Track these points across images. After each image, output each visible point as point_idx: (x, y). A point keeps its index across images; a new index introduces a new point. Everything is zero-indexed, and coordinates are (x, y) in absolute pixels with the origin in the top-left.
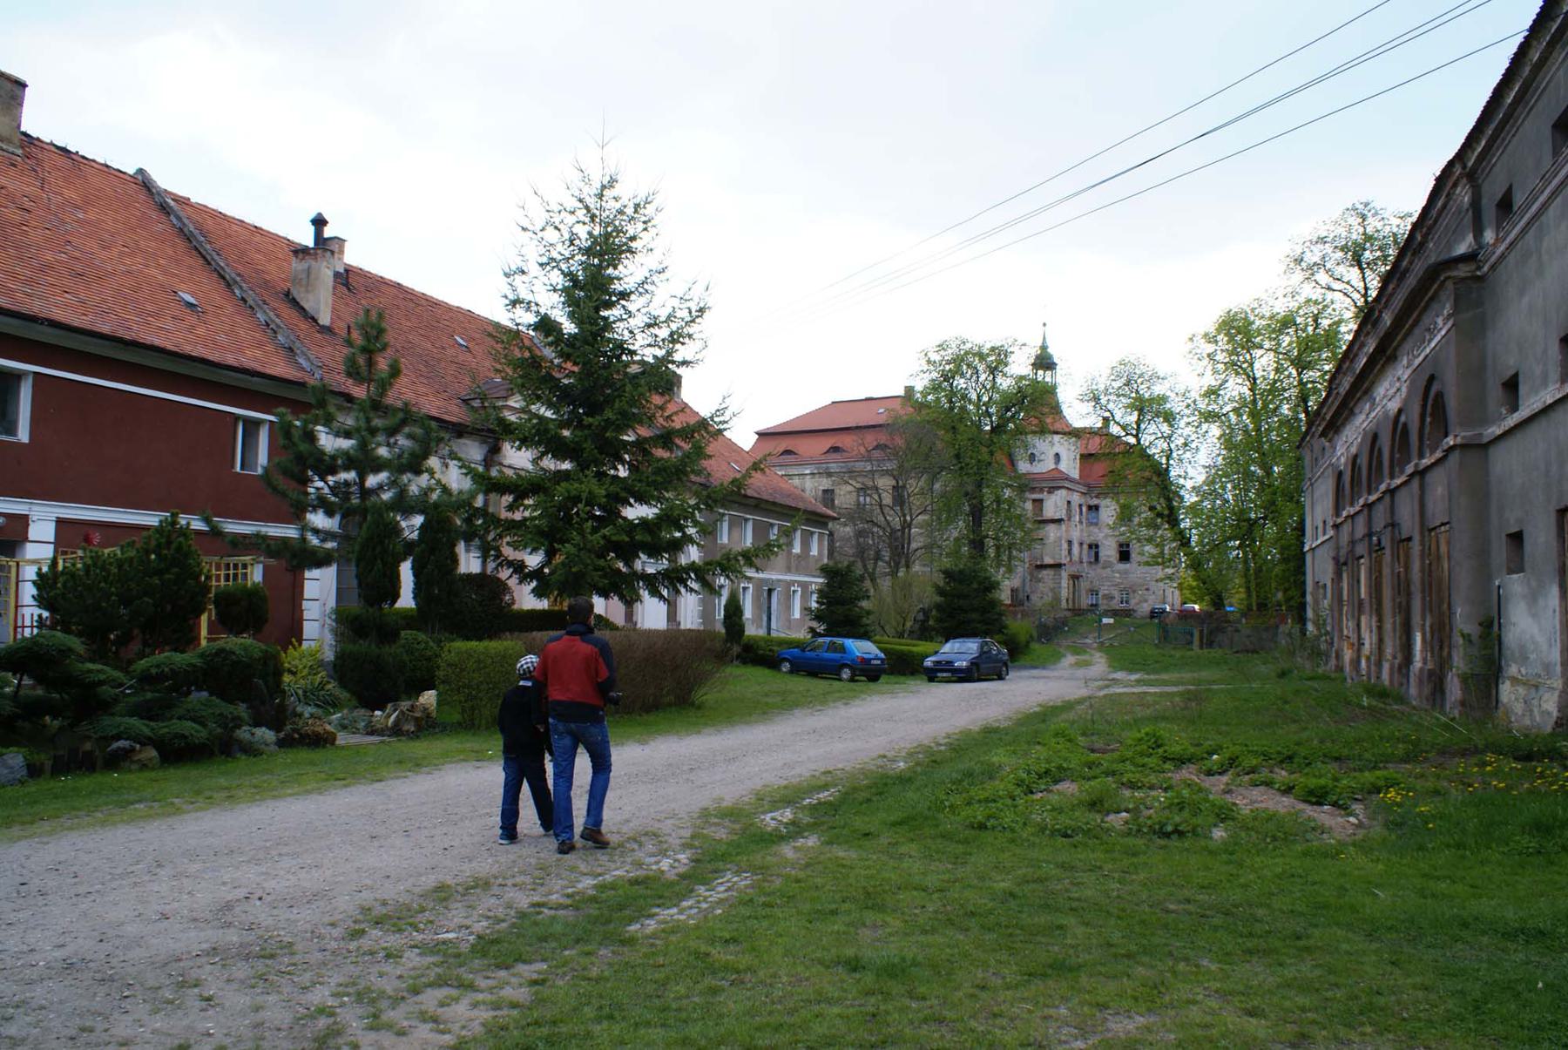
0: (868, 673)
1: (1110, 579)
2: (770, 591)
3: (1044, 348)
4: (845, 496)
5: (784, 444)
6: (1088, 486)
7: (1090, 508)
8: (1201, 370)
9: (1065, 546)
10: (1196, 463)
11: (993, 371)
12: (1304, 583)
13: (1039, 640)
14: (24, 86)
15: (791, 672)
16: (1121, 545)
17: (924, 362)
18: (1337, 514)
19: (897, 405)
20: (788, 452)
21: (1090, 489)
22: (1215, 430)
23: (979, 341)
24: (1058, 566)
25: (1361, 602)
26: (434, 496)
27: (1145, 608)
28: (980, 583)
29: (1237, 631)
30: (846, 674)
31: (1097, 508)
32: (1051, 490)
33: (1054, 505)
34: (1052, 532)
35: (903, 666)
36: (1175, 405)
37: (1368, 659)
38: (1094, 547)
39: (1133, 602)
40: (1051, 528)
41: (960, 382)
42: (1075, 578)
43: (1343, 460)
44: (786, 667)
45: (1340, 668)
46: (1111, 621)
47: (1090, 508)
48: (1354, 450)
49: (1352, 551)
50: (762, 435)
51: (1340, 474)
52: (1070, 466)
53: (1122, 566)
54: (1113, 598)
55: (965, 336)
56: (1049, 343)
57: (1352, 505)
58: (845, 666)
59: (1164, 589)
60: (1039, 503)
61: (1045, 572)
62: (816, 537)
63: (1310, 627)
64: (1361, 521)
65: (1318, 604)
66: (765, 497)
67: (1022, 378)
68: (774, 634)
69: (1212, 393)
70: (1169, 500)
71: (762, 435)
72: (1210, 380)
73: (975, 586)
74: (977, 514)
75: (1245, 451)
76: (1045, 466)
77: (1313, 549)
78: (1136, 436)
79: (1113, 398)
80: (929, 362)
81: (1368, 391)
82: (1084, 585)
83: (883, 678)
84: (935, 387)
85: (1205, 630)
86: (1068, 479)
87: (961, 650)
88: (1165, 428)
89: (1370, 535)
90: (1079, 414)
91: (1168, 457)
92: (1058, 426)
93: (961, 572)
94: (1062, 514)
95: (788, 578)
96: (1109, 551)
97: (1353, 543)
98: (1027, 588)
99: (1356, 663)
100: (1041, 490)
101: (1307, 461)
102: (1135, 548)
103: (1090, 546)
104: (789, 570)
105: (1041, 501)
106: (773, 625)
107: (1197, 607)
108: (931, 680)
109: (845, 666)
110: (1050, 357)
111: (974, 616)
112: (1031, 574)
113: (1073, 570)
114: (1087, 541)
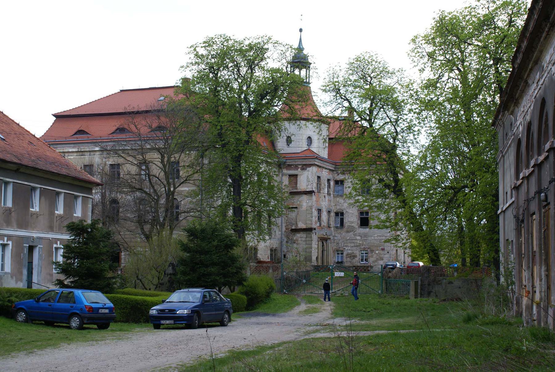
0: (97, 321)
1: (353, 242)
2: (31, 249)
3: (300, 49)
4: (129, 168)
5: (76, 125)
6: (335, 164)
7: (337, 182)
8: (421, 66)
9: (315, 213)
10: (417, 140)
11: (251, 66)
12: (498, 240)
13: (281, 291)
15: (26, 321)
16: (362, 213)
17: (192, 56)
18: (517, 178)
19: (171, 92)
20: (80, 132)
21: (336, 167)
22: (431, 117)
23: (239, 38)
24: (309, 230)
25: (534, 252)
27: (378, 267)
28: (220, 241)
29: (451, 283)
30: (75, 322)
32: (305, 167)
33: (307, 179)
34: (304, 202)
35: (136, 315)
36: (400, 96)
37: (538, 305)
38: (340, 214)
39: (371, 260)
40: (304, 197)
41: (224, 74)
42: (324, 240)
43: (521, 128)
44: (22, 316)
45: (519, 314)
46: (342, 274)
47: (337, 182)
48: (528, 118)
49: (527, 209)
50: (59, 117)
51: (519, 141)
52: (320, 148)
54: (355, 256)
55: (229, 34)
56: (304, 45)
57: (527, 167)
58: (74, 314)
59: (397, 252)
60: (294, 177)
61: (298, 235)
62: (80, 201)
63: (502, 279)
64: (533, 180)
65: (508, 257)
66: (25, 162)
67: (277, 71)
68: (35, 287)
69: (431, 85)
70: (395, 174)
71: (59, 117)
72: (429, 74)
73: (215, 243)
74: (238, 184)
75: (451, 134)
76: (299, 146)
77: (504, 212)
78: (369, 121)
79: (351, 89)
80: (197, 55)
81: (538, 61)
82: (331, 247)
83: (112, 326)
84: (202, 78)
85: (426, 282)
86: (318, 158)
87: (184, 299)
88: (391, 113)
89: (539, 192)
90: (325, 103)
91: (395, 139)
92: (307, 112)
93: (203, 231)
94: (313, 187)
95: (50, 236)
96: (352, 217)
97: (528, 201)
98: (284, 249)
99: (529, 308)
100: (296, 167)
101: (500, 135)
102: (373, 214)
103: (337, 214)
104: (51, 229)
105: (296, 176)
106: (35, 279)
107: (421, 264)
108: (157, 327)
109: (74, 314)
110: (306, 57)
111: (213, 269)
112: (288, 237)
113: (322, 233)
114: (334, 209)
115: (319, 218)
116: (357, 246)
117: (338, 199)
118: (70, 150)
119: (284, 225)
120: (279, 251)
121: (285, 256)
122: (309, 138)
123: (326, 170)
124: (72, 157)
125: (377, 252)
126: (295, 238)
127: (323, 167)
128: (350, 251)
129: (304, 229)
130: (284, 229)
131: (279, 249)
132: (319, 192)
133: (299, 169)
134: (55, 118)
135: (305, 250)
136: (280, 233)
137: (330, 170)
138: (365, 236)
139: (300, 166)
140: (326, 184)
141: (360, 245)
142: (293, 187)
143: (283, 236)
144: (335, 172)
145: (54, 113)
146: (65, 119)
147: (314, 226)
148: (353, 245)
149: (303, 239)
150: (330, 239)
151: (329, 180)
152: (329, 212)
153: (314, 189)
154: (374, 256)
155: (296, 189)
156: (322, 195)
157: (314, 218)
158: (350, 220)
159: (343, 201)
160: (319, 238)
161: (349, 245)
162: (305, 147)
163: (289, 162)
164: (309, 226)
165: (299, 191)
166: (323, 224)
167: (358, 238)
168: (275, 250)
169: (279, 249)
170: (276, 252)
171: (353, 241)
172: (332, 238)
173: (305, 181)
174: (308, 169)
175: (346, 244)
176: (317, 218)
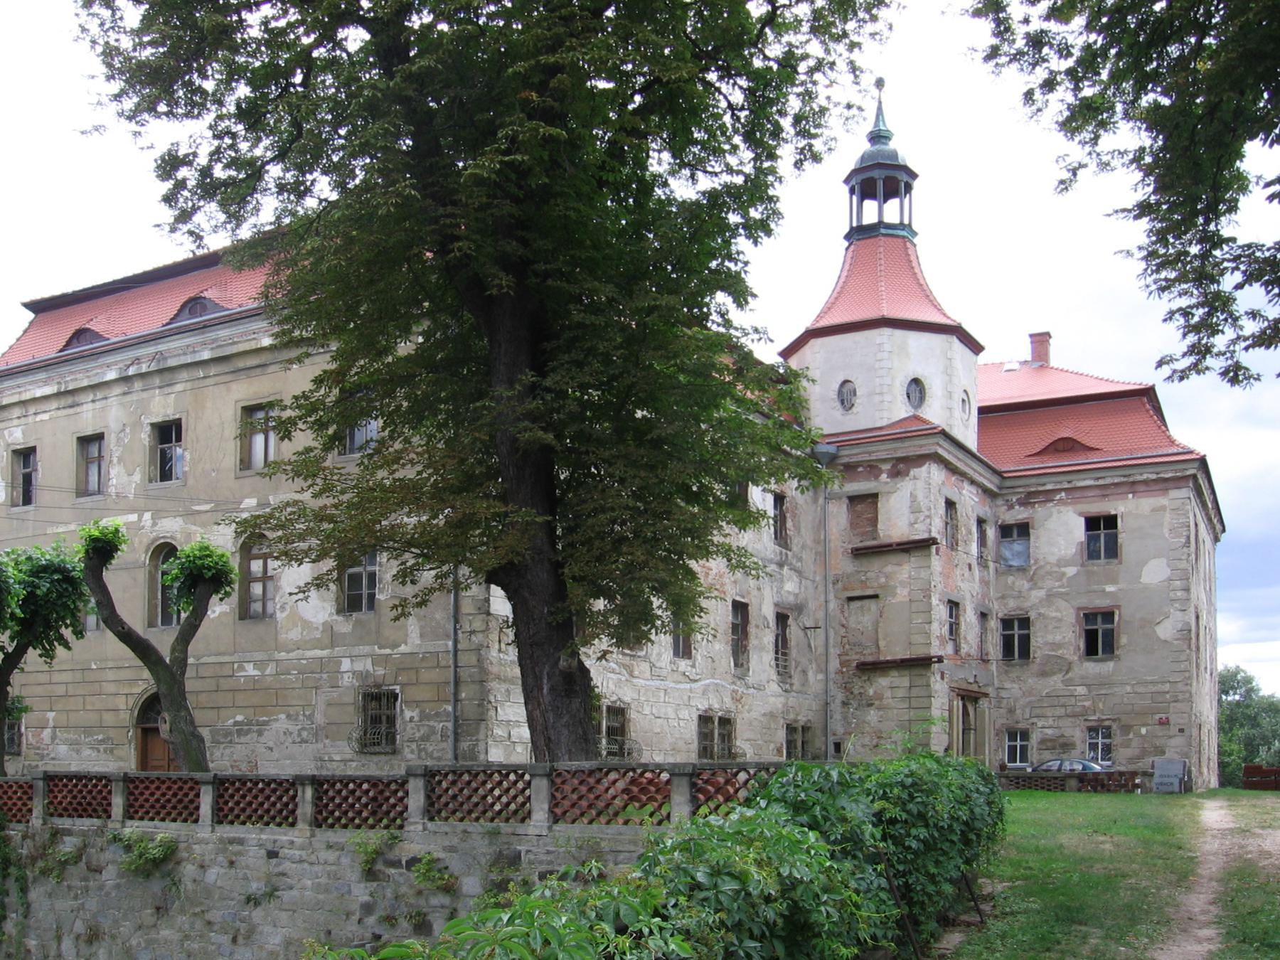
9: (941, 612)
14: (914, 176)
24: (922, 663)
26: (287, 221)
31: (1024, 529)
32: (902, 466)
33: (909, 505)
40: (903, 571)
42: (969, 697)
53: (1092, 668)
60: (865, 504)
61: (883, 682)
71: (40, 307)
82: (991, 716)
96: (1058, 632)
98: (837, 726)
100: (872, 469)
103: (1007, 623)
105: (874, 497)
112: (847, 688)
113: (966, 675)
114: (999, 610)
115: (954, 629)
116: (1074, 716)
117: (1010, 579)
118: (39, 393)
119: (834, 652)
120: (819, 733)
121: (838, 747)
122: (916, 382)
123: (973, 489)
124: (45, 417)
125: (1143, 731)
126: (871, 692)
127: (963, 475)
128: (1049, 731)
129: (903, 661)
130: (834, 664)
131: (817, 727)
132: (953, 546)
133: (884, 476)
134: (30, 316)
135: (907, 726)
136: (820, 677)
137: (986, 491)
138: (1102, 685)
139: (886, 467)
140: (974, 529)
141: (1084, 713)
142: (863, 534)
143: (831, 685)
144: (1000, 502)
145: (27, 300)
146: (63, 311)
147: (935, 650)
148: (1061, 711)
149: (901, 693)
150: (986, 695)
151: (981, 522)
152: (983, 616)
153: (934, 534)
154: (1135, 743)
155: (874, 539)
156: (960, 557)
157: (935, 626)
158: (1050, 638)
159: (1026, 585)
160: (952, 689)
161: (1049, 712)
162: (901, 410)
163: (848, 455)
164: (919, 652)
165: (887, 541)
166: (965, 649)
167: (1081, 690)
168: (805, 729)
169: (817, 727)
170: (809, 735)
171: (1063, 700)
172: (990, 690)
173: (906, 511)
174: (914, 472)
175: (1038, 711)
176: (947, 627)
